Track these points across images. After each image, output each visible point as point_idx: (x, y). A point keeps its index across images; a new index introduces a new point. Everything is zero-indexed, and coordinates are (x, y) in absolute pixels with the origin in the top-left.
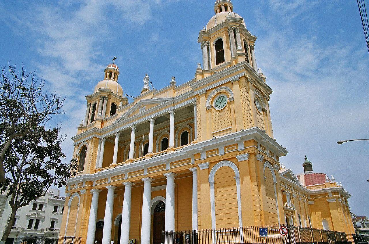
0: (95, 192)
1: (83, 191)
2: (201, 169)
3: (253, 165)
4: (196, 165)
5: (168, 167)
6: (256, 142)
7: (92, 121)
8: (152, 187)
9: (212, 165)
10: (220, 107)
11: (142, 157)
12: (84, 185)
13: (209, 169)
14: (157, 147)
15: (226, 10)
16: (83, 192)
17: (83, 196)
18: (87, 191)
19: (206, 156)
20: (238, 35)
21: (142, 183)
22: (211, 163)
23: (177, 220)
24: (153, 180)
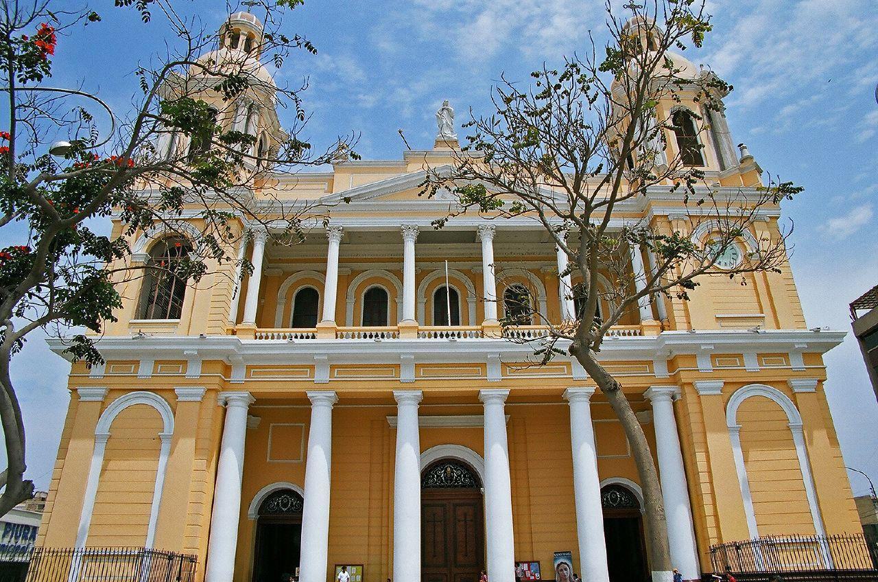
2: (82, 399)
5: (322, 375)
9: (115, 394)
20: (255, 118)
23: (382, 517)
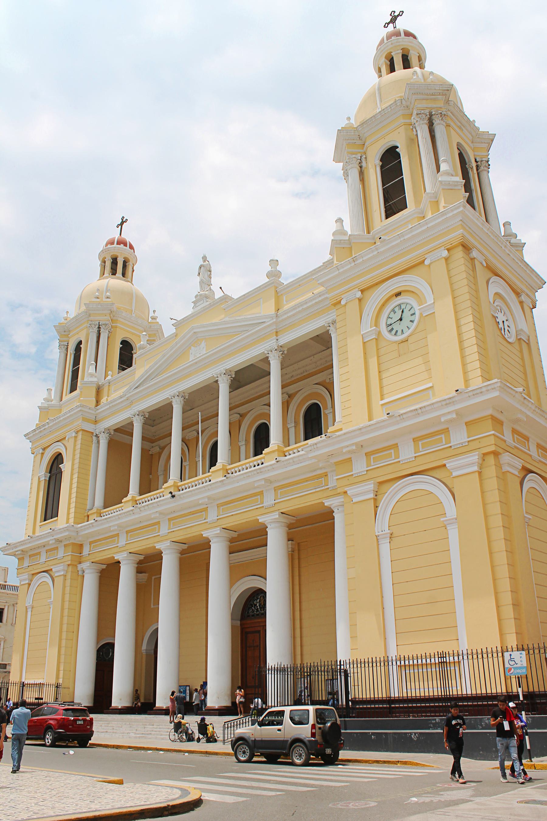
0: (273, 525)
1: (58, 570)
3: (492, 483)
4: (339, 491)
6: (497, 422)
7: (73, 388)
8: (230, 554)
10: (399, 332)
11: (201, 476)
12: (61, 553)
13: (375, 500)
14: (292, 431)
15: (407, 64)
16: (59, 571)
17: (59, 581)
18: (70, 567)
19: (365, 466)
21: (206, 545)
22: (381, 483)
24: (292, 520)
